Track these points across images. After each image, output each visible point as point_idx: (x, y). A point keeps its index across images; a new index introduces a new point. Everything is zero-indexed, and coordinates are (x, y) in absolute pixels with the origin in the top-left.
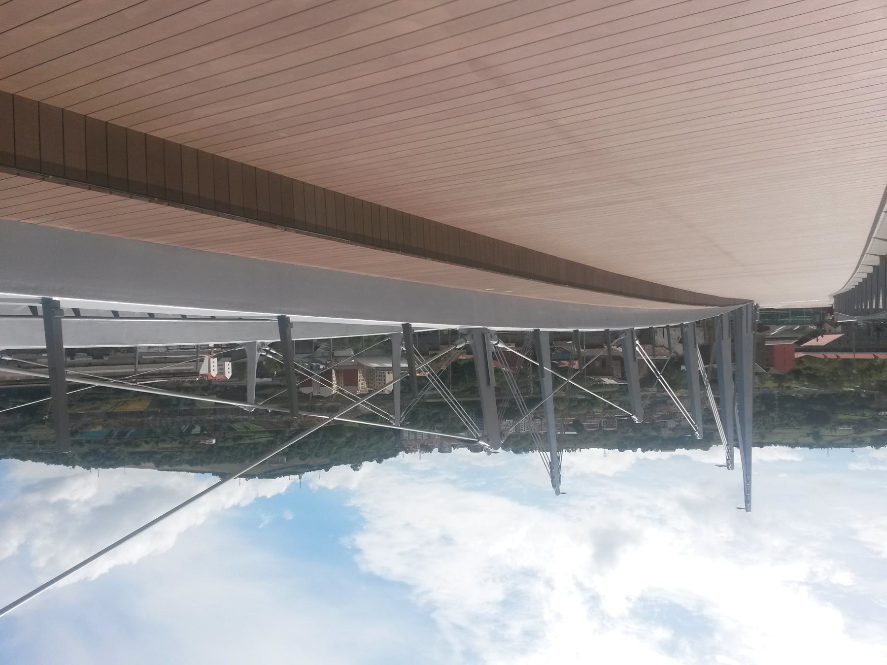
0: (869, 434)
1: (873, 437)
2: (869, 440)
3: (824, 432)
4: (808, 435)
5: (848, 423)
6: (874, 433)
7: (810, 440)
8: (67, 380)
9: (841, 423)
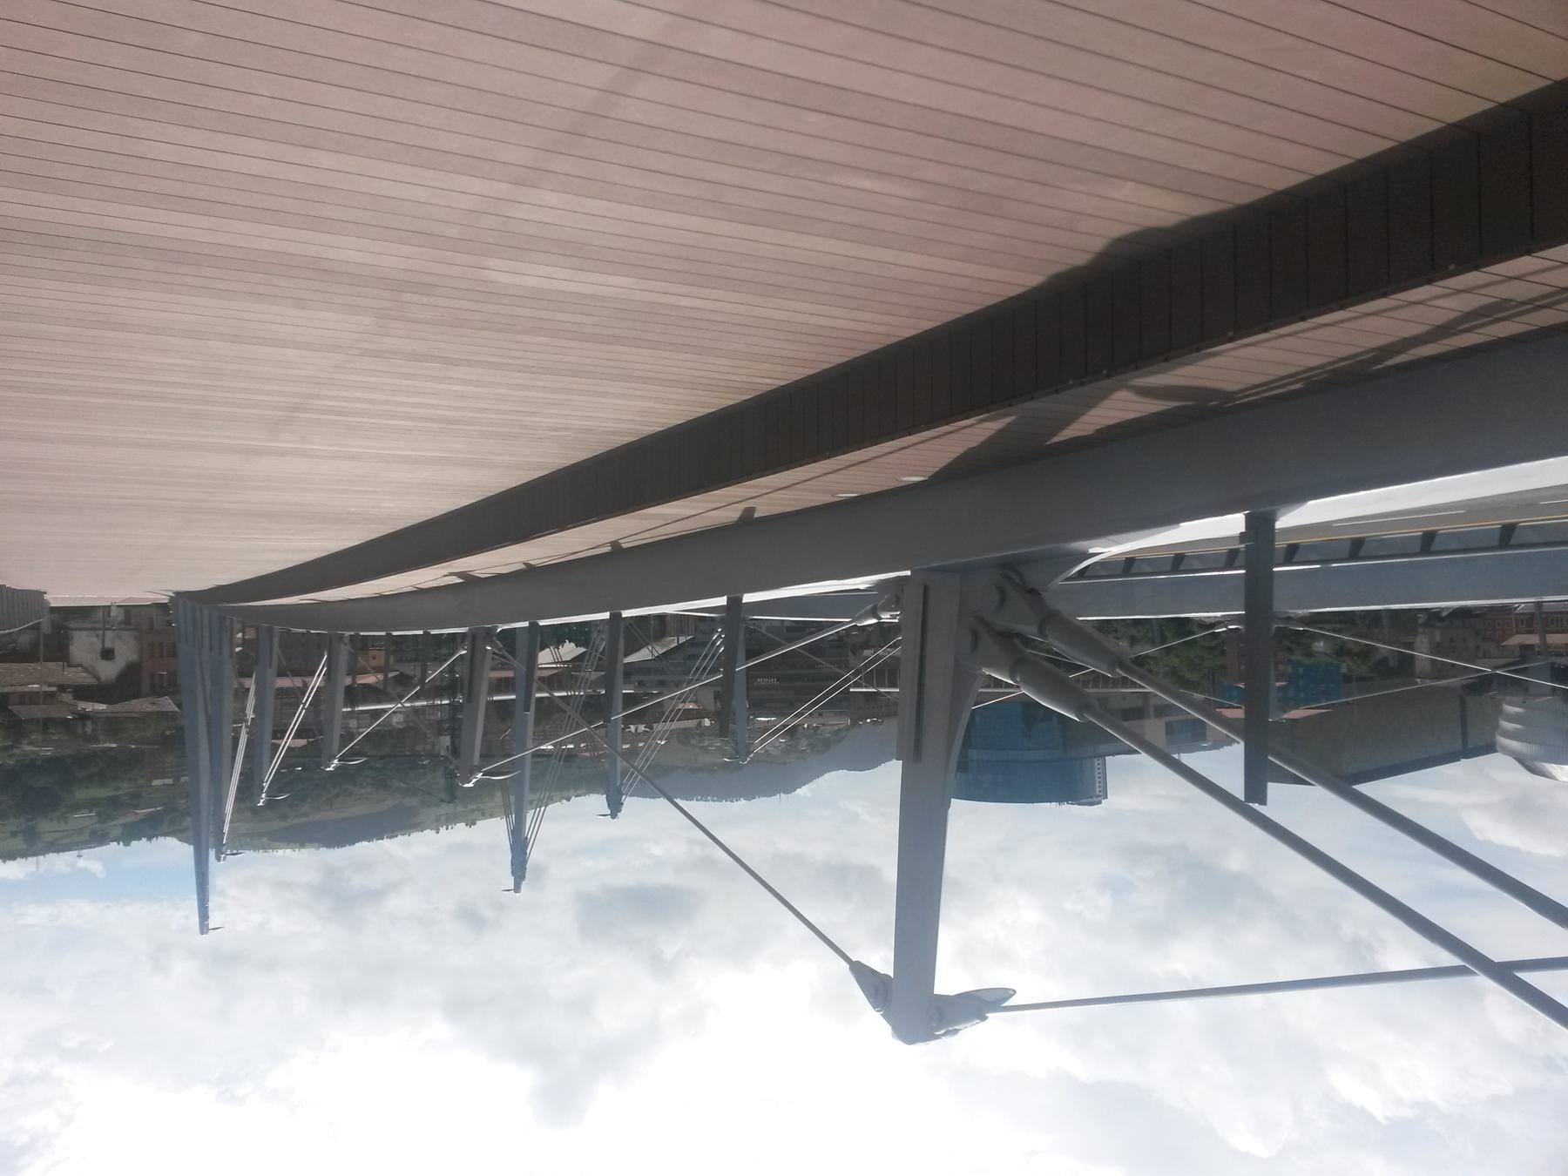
0: (123, 820)
1: (125, 825)
2: (117, 832)
3: (46, 826)
4: (14, 834)
5: (92, 804)
6: (130, 819)
7: (18, 843)
8: (908, 573)
9: (77, 807)
